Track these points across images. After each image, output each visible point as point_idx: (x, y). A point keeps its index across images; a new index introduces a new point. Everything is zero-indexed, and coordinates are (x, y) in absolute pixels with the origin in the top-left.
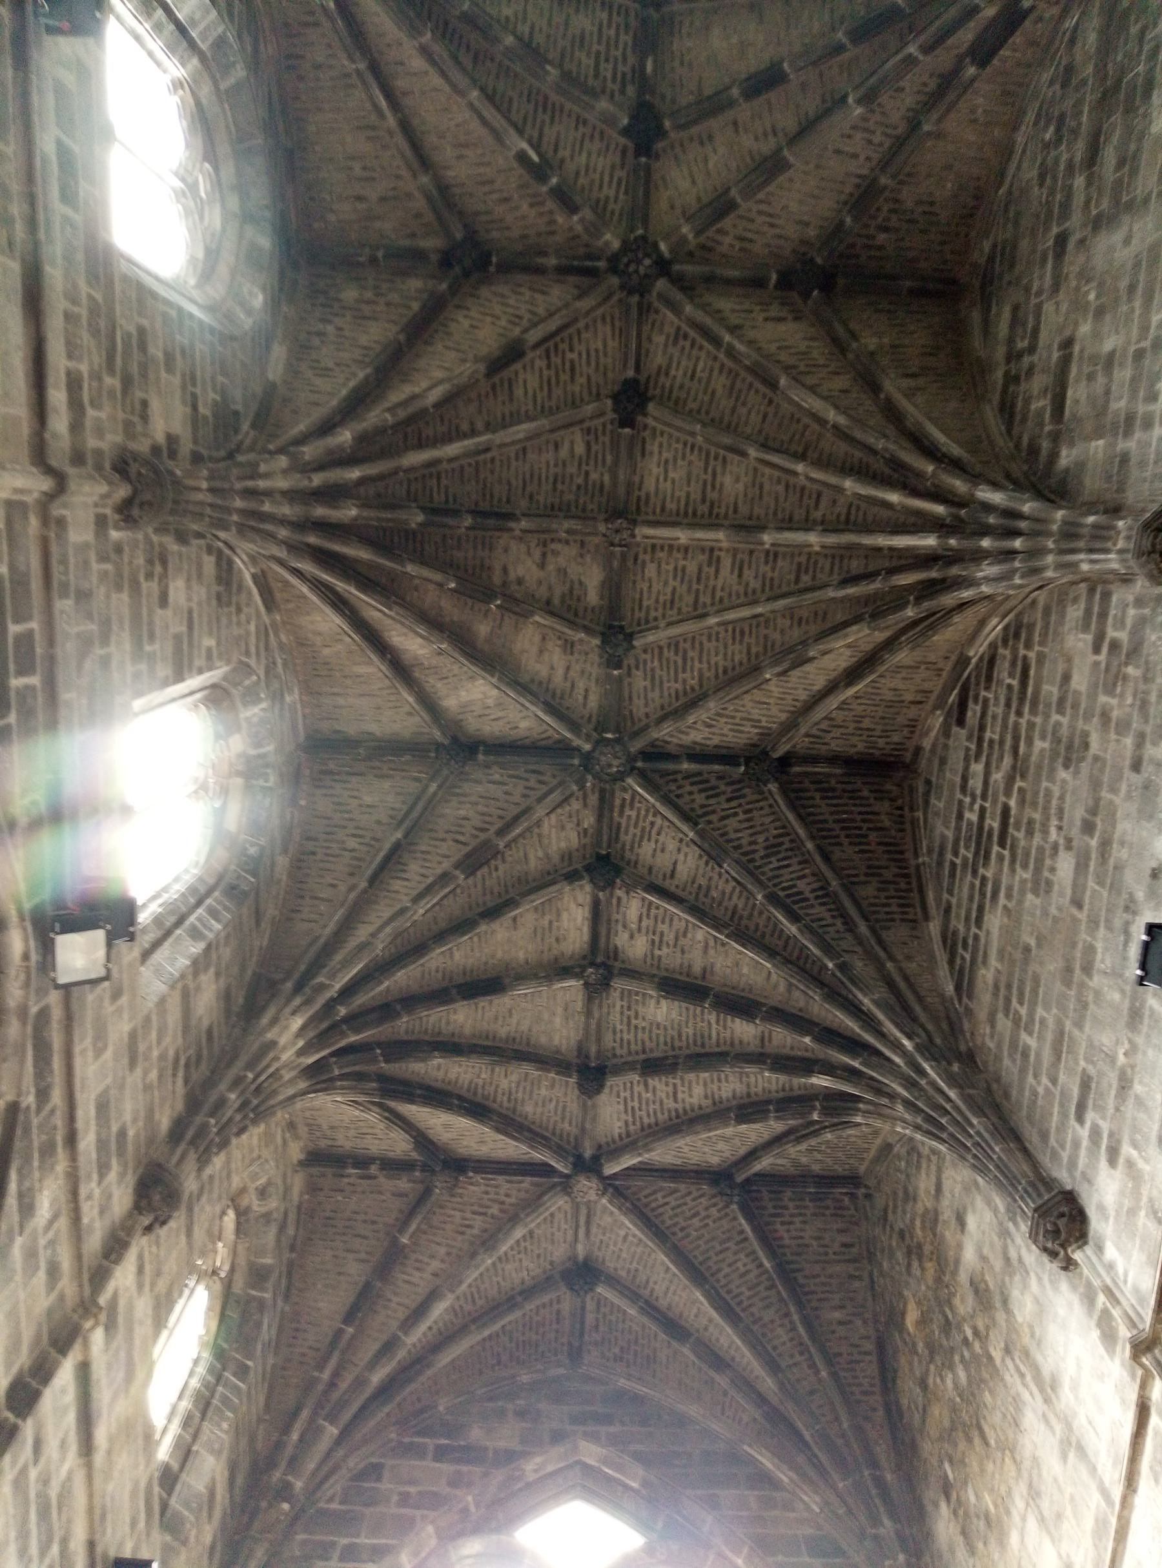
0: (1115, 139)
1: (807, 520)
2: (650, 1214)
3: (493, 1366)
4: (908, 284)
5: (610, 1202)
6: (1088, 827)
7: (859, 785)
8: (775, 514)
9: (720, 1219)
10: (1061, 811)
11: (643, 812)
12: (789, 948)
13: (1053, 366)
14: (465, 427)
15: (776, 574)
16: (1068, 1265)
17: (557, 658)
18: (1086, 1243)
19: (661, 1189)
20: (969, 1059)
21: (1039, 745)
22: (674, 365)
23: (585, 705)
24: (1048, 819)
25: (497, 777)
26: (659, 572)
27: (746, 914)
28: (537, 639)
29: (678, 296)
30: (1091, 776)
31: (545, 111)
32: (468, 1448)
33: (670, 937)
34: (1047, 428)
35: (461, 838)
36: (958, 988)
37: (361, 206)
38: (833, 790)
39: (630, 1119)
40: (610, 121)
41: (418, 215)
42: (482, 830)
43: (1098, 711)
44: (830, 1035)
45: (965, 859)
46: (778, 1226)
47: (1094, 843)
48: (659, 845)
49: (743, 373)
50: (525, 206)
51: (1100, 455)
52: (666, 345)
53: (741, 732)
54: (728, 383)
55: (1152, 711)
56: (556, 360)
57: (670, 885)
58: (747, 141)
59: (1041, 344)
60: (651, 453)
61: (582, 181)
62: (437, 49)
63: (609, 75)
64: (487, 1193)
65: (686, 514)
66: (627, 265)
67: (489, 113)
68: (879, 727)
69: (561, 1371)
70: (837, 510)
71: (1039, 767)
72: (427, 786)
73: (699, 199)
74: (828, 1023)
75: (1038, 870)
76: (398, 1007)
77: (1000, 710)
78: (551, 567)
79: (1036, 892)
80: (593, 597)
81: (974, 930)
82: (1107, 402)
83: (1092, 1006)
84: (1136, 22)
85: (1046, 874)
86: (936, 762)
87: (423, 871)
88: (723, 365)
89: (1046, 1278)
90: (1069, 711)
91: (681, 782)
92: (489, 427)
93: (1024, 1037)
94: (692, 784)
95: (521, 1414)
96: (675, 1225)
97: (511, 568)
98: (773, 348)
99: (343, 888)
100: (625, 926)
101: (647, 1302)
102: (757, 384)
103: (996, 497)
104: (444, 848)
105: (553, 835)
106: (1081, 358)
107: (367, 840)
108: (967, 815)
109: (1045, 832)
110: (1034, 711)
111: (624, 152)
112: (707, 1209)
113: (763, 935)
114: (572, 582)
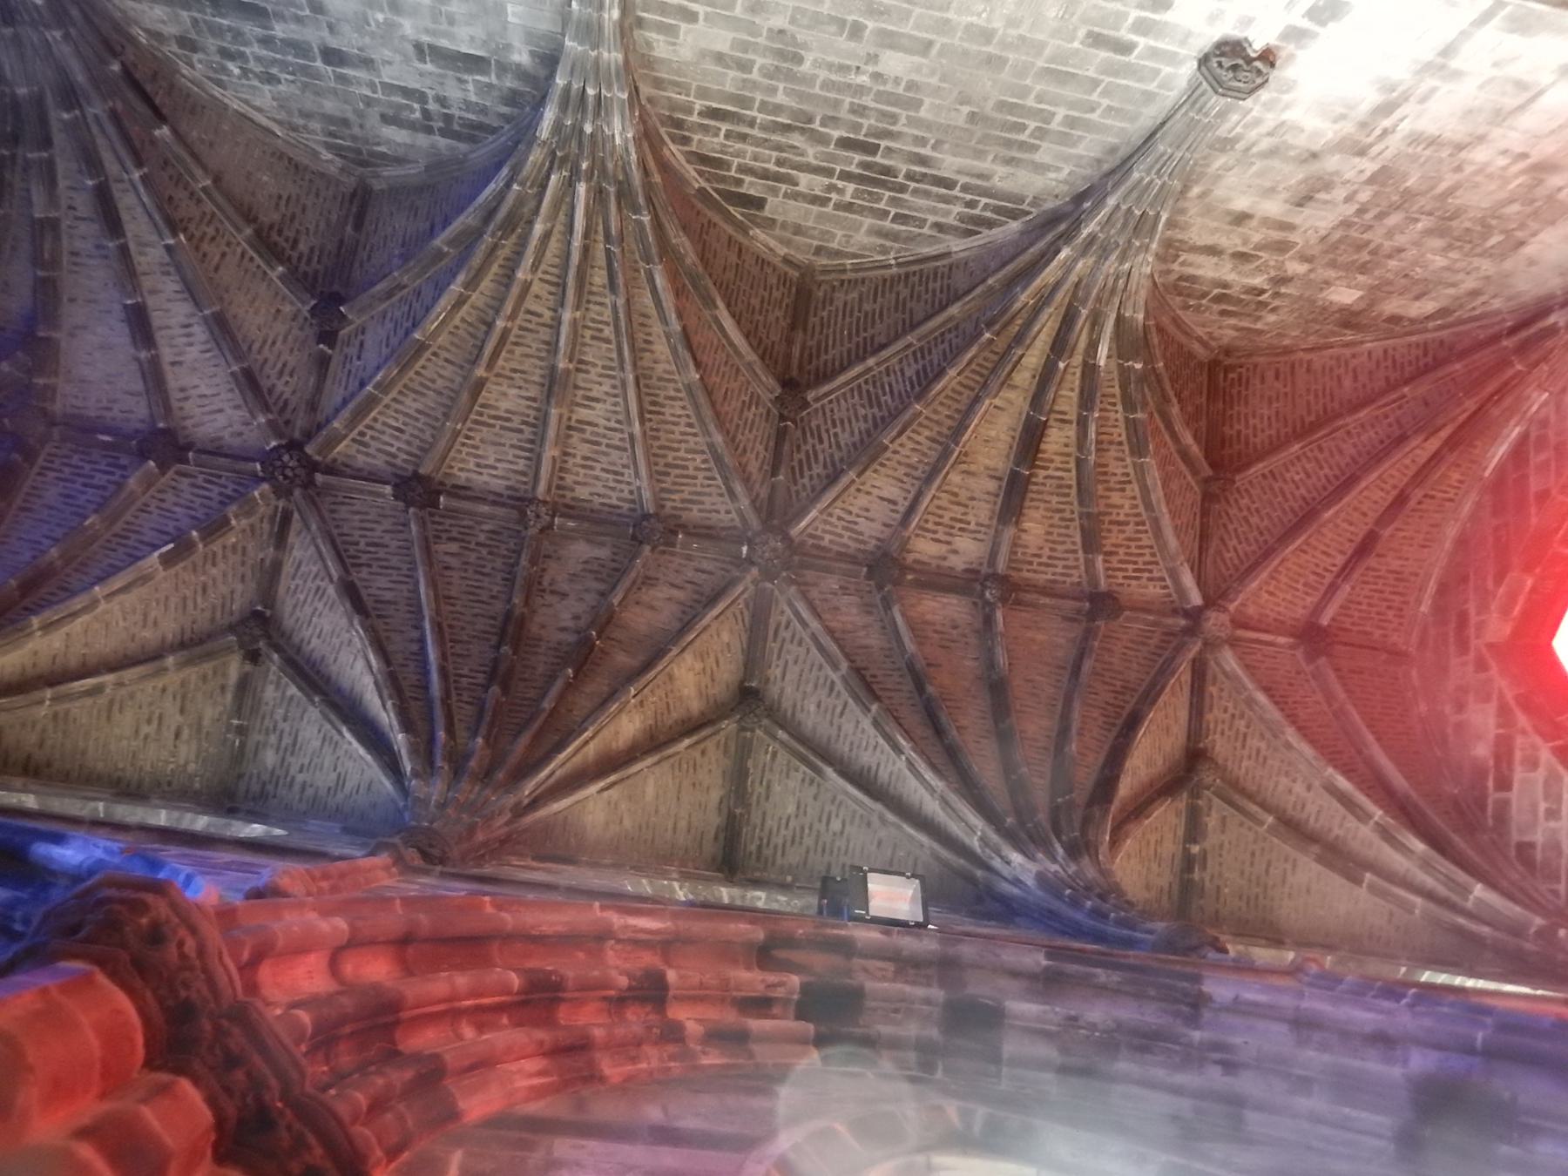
2: (1246, 565)
4: (349, 229)
5: (1232, 601)
7: (816, 320)
8: (541, 359)
9: (1250, 496)
10: (843, 69)
11: (828, 527)
12: (972, 384)
14: (415, 647)
15: (600, 363)
16: (1268, 57)
17: (660, 594)
18: (1246, 39)
19: (1219, 552)
20: (1080, 198)
21: (780, 98)
22: (388, 448)
23: (710, 573)
24: (849, 86)
25: (778, 672)
26: (585, 484)
27: (936, 428)
28: (637, 609)
29: (320, 439)
30: (809, 27)
31: (127, 538)
32: (1498, 758)
33: (957, 511)
34: (493, 79)
35: (839, 710)
36: (1014, 215)
37: (186, 733)
39: (1146, 575)
40: (149, 483)
41: (204, 678)
42: (832, 689)
44: (1060, 346)
46: (1258, 440)
47: (871, 25)
49: (405, 380)
50: (214, 571)
52: (367, 454)
53: (753, 422)
56: (364, 558)
57: (902, 506)
58: (193, 353)
59: (417, 86)
60: (468, 480)
62: (50, 615)
64: (1222, 733)
65: (531, 450)
66: (286, 477)
67: (118, 582)
69: (1414, 673)
70: (544, 294)
71: (802, 97)
72: (782, 743)
73: (237, 407)
74: (1047, 348)
77: (750, 149)
78: (565, 587)
79: (918, 104)
81: (956, 192)
85: (900, 90)
87: (871, 748)
88: (394, 400)
90: (750, 56)
92: (419, 627)
93: (1054, 125)
94: (802, 477)
95: (1460, 707)
96: (1257, 541)
97: (563, 624)
100: (945, 558)
101: (1338, 576)
103: (549, 114)
104: (848, 727)
105: (844, 618)
106: (433, 33)
107: (834, 808)
108: (848, 198)
109: (860, 90)
112: (1240, 510)
113: (957, 411)
114: (584, 570)
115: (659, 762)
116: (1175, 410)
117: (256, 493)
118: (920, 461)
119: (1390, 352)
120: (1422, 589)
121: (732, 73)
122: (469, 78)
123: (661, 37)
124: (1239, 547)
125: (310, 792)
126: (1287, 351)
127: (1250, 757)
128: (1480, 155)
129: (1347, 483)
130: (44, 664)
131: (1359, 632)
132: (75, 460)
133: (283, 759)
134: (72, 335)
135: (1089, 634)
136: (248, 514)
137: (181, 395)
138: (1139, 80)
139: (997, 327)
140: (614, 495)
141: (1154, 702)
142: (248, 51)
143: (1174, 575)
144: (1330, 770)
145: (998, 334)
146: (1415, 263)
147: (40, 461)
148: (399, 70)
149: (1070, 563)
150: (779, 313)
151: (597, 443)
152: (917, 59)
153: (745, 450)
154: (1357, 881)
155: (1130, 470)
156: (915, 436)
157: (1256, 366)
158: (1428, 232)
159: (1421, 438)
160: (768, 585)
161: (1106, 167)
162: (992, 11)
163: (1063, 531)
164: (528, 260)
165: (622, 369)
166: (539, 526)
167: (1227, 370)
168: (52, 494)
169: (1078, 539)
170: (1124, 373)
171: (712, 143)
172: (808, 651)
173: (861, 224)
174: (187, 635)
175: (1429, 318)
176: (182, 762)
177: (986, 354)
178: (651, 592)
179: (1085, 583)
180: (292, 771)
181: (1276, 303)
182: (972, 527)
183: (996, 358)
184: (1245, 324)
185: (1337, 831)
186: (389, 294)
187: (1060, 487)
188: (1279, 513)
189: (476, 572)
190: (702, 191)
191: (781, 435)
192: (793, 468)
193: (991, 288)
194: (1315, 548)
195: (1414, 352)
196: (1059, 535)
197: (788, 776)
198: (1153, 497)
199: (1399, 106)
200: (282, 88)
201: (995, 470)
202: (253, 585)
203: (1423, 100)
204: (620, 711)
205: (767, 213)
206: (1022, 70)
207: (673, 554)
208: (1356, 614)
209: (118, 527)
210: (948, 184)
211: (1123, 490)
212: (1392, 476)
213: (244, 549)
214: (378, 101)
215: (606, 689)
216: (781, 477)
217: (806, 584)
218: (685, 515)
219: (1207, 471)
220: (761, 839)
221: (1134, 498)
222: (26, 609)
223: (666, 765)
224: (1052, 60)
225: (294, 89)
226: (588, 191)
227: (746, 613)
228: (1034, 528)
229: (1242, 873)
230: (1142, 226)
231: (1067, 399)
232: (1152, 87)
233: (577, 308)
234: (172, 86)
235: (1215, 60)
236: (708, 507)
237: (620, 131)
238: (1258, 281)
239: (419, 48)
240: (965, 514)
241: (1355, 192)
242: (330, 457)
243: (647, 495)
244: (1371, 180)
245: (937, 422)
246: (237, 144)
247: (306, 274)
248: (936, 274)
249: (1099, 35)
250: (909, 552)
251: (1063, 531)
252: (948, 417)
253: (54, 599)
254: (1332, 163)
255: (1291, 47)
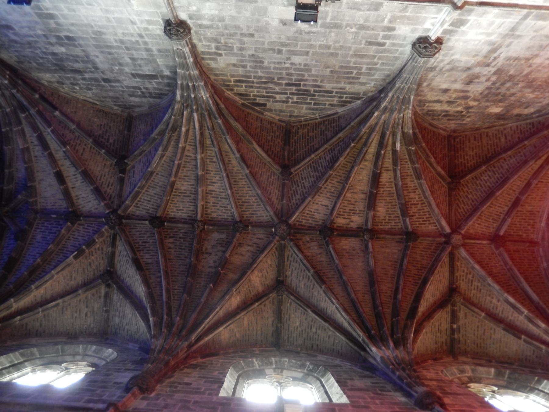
0: (71, 64)
1: (195, 160)
2: (468, 214)
3: (540, 278)
5: (462, 229)
6: (280, 52)
8: (193, 171)
9: (468, 187)
11: (303, 217)
12: (351, 161)
13: (141, 80)
14: (159, 280)
15: (214, 170)
16: (439, 41)
18: (428, 36)
20: (381, 91)
21: (260, 74)
22: (146, 208)
23: (262, 239)
25: (290, 273)
26: (215, 212)
27: (340, 178)
28: (236, 256)
29: (123, 207)
30: (262, 53)
31: (63, 250)
33: (351, 207)
34: (160, 80)
35: (312, 287)
36: (358, 99)
37: (89, 315)
38: (295, 149)
39: (428, 222)
40: (69, 230)
41: (93, 295)
42: (309, 279)
43: (240, 52)
44: (381, 145)
45: (311, 99)
46: (469, 165)
47: (284, 49)
48: (316, 211)
49: (149, 184)
50: (93, 258)
51: (161, 60)
52: (140, 210)
53: (273, 182)
54: (152, 189)
55: (232, 32)
57: (330, 208)
58: (78, 184)
59: (137, 85)
60: (174, 215)
61: (86, 238)
62: (37, 284)
63: (55, 229)
64: (463, 280)
65: (195, 203)
66: (112, 223)
67: (59, 268)
68: (271, 134)
69: (541, 249)
70: (191, 149)
71: (267, 73)
73: (95, 200)
74: (377, 145)
75: (302, 70)
76: (376, 311)
77: (255, 90)
78: (210, 250)
79: (310, 70)
80: (223, 236)
81: (334, 94)
82: (145, 59)
83: (341, 44)
84: (38, 60)
85: (302, 67)
86: (281, 113)
87: (324, 301)
88: (146, 191)
89: (451, 52)
90: (245, 63)
91: (292, 204)
92: (160, 272)
93: (363, 70)
94: (293, 200)
96: (471, 204)
98: (141, 174)
99: (330, 333)
100: (348, 224)
101: (506, 215)
102: (152, 179)
103: (178, 93)
104: (316, 293)
107: (313, 323)
108: (295, 100)
109: (287, 69)
110: (249, 77)
111: (79, 224)
113: (347, 171)
115: (246, 313)
116: (433, 160)
117: (103, 230)
118: (335, 190)
119: (519, 127)
120: (541, 217)
121: (240, 69)
122: (153, 81)
123: (212, 62)
124: (465, 207)
125: (130, 333)
126: (478, 129)
127: (474, 289)
128: (538, 61)
129: (504, 181)
130: (39, 299)
131: (517, 235)
132: (46, 224)
133: (121, 321)
134: (39, 183)
135: (406, 248)
136: (102, 236)
137: (76, 198)
138: (391, 53)
139: (356, 141)
140: (225, 215)
141: (433, 273)
142: (79, 82)
143: (438, 221)
144: (506, 295)
145: (357, 143)
146: (522, 97)
147: (35, 226)
148: (128, 82)
149: (397, 221)
150: (279, 140)
151: (217, 198)
152: (305, 57)
153: (270, 193)
154: (520, 338)
155: (417, 184)
156: (332, 182)
157: (466, 136)
158: (524, 87)
159: (533, 161)
160: (283, 242)
161: (387, 81)
162: (327, 39)
163: (393, 210)
164: (182, 140)
165: (221, 172)
166: (199, 230)
167: (455, 138)
168: (39, 237)
169: (399, 212)
170: (409, 152)
171: (242, 89)
172: (300, 265)
173: (303, 107)
174: (86, 281)
175: (532, 114)
176: (88, 324)
177: (355, 150)
178: (241, 249)
179: (404, 228)
180: (124, 325)
181: (469, 114)
182: (358, 212)
183: (358, 151)
184: (458, 122)
185: (510, 318)
186: (140, 154)
187: (390, 194)
188: (480, 193)
189: (179, 248)
190: (243, 104)
191: (284, 185)
192: (289, 197)
193: (353, 126)
194: (496, 205)
195: (529, 126)
196: (392, 211)
197: (296, 311)
198: (427, 194)
199: (498, 49)
200: (94, 91)
201: (364, 190)
202: (106, 260)
203: (508, 46)
204: (230, 298)
205: (268, 107)
206: (346, 56)
207: (248, 233)
208: (515, 229)
209: (60, 247)
210: (331, 92)
211: (415, 192)
212: (524, 175)
213: (102, 249)
214: (125, 91)
215: (226, 288)
216: (284, 202)
217: (298, 239)
218: (251, 219)
219: (450, 180)
220: (288, 335)
221: (420, 194)
222: (32, 281)
223: (251, 313)
224: (354, 52)
225: (97, 91)
226: (198, 115)
227: (277, 252)
228: (381, 210)
229: (474, 334)
230: (405, 101)
231: (388, 162)
232: (397, 55)
233: (202, 153)
234: (59, 96)
235: (417, 45)
236: (259, 215)
237: (204, 95)
238: (459, 109)
239: (133, 75)
240: (354, 207)
241: (489, 78)
242: (127, 214)
243: (236, 215)
244: (495, 73)
245: (340, 176)
246: (84, 110)
247: (113, 150)
248: (334, 120)
249: (370, 42)
250: (335, 223)
251: (393, 210)
252: (343, 173)
253: (41, 276)
254: (477, 70)
255: (448, 36)
